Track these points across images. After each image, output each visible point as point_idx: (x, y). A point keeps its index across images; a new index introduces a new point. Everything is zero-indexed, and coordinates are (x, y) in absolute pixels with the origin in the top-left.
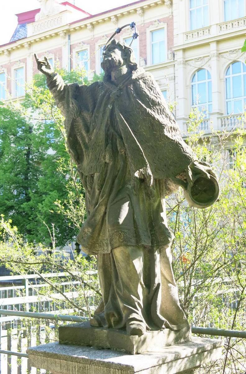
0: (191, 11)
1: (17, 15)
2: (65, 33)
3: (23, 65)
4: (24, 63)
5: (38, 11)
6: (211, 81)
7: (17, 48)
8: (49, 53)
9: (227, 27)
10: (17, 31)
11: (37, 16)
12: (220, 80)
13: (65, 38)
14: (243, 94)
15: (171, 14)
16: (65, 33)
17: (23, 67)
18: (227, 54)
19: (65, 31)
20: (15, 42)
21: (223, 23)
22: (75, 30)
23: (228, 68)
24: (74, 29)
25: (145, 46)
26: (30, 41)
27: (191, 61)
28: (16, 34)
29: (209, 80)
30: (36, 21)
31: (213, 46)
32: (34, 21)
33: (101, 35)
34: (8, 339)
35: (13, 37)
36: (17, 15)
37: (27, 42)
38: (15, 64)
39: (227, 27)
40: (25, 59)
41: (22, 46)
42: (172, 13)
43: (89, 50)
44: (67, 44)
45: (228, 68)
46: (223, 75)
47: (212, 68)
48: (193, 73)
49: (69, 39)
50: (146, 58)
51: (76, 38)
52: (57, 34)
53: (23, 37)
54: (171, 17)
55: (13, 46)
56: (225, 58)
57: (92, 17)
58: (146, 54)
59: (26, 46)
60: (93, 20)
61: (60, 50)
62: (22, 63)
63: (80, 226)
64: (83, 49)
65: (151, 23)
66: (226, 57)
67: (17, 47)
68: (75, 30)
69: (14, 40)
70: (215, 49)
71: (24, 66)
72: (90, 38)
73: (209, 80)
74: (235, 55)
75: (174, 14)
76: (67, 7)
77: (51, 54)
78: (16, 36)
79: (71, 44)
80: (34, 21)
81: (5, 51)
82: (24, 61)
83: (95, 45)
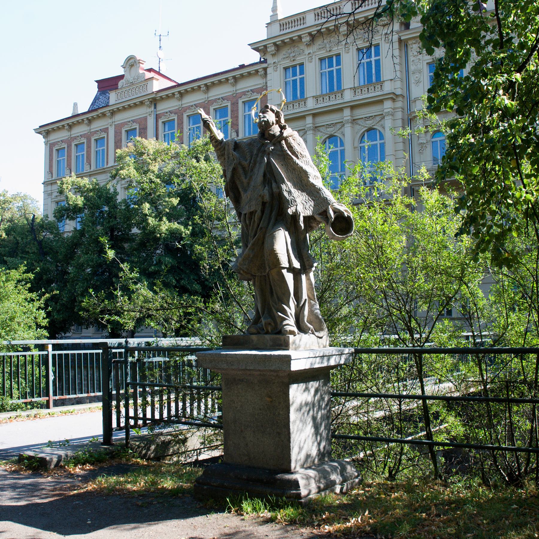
0: (321, 74)
1: (96, 81)
2: (151, 102)
3: (104, 135)
4: (105, 132)
5: (122, 77)
6: (344, 150)
7: (98, 117)
8: (224, 100)
9: (361, 92)
10: (96, 99)
11: (121, 83)
12: (354, 148)
13: (150, 107)
14: (340, 170)
15: (265, 84)
16: (151, 102)
17: (136, 128)
18: (323, 127)
19: (151, 100)
20: (96, 110)
21: (320, 96)
22: (162, 98)
23: (363, 136)
24: (161, 97)
25: (237, 117)
26: (113, 110)
27: (360, 120)
28: (95, 102)
29: (342, 148)
30: (119, 88)
31: (347, 112)
32: (117, 88)
33: (216, 97)
34: (104, 406)
35: (93, 104)
36: (96, 81)
37: (109, 110)
38: (95, 133)
39: (361, 92)
40: (107, 128)
41: (104, 115)
42: (266, 83)
43: (85, 143)
44: (153, 113)
45: (363, 136)
46: (357, 144)
47: (346, 135)
48: (324, 140)
49: (155, 108)
50: (238, 130)
51: (163, 107)
52: (142, 103)
53: (104, 105)
54: (264, 87)
55: (94, 114)
56: (360, 125)
57: (179, 85)
58: (238, 125)
59: (108, 114)
60: (182, 89)
61: (145, 119)
62: (135, 124)
63: (174, 298)
64: (101, 137)
65: (244, 93)
66: (322, 130)
67: (97, 115)
68: (162, 98)
69: (93, 108)
70: (311, 122)
71: (106, 136)
72: (177, 108)
73: (342, 148)
74: (332, 129)
75: (268, 85)
76: (152, 74)
77: (226, 101)
78: (96, 104)
79: (157, 113)
80: (117, 88)
81: (85, 120)
82: (106, 130)
83: (183, 115)
